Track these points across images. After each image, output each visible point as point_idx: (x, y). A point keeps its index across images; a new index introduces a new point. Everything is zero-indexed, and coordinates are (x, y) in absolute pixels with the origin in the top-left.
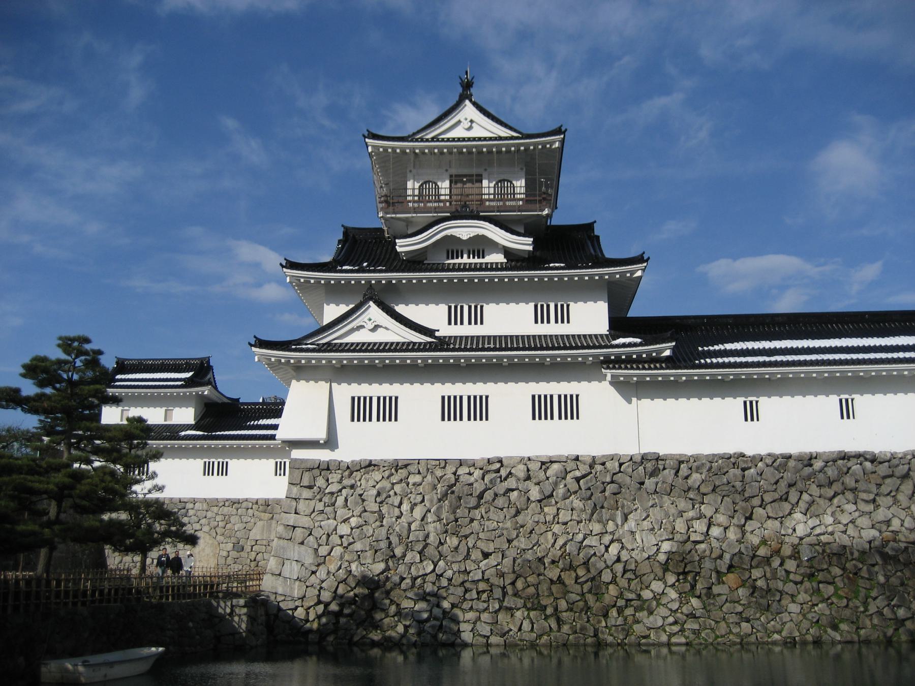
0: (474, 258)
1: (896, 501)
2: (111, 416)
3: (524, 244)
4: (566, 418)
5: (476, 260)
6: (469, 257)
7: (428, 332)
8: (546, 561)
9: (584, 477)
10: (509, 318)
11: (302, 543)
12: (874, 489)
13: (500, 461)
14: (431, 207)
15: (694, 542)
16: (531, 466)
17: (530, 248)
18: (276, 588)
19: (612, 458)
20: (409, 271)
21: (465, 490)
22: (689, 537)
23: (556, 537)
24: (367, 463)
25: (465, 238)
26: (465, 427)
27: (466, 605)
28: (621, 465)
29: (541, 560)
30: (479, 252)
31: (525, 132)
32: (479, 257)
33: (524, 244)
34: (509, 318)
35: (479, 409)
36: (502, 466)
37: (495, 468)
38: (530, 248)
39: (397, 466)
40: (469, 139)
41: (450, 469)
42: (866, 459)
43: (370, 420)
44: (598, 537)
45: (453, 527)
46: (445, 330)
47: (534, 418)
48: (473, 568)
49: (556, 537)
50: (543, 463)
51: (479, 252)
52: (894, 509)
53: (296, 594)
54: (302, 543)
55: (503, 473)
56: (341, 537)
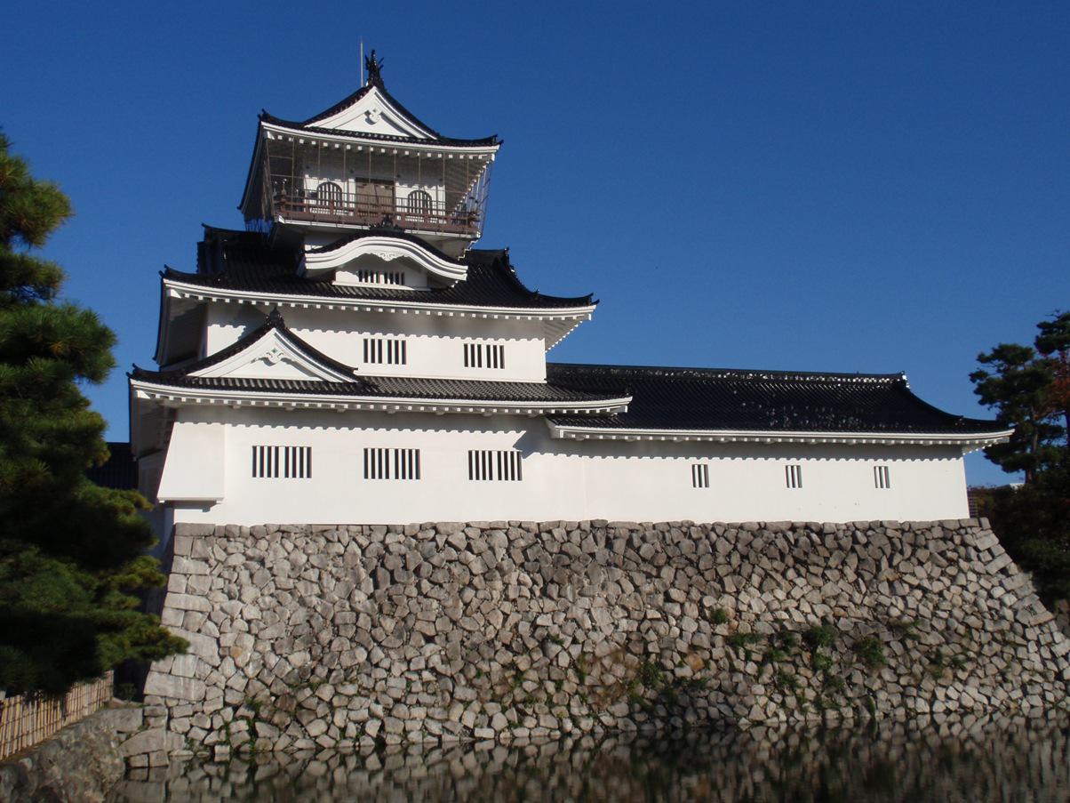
0: (392, 283)
1: (843, 575)
2: (1016, 481)
3: (459, 273)
4: (506, 478)
5: (395, 287)
6: (386, 282)
7: (347, 371)
8: (498, 644)
9: (530, 546)
10: (433, 356)
11: (199, 631)
12: (822, 563)
13: (435, 528)
14: (314, 215)
15: (651, 620)
16: (470, 532)
17: (464, 277)
18: (165, 690)
19: (558, 524)
20: (965, 432)
21: (399, 565)
22: (645, 615)
23: (506, 616)
24: (276, 529)
25: (387, 260)
26: (282, 485)
27: (412, 699)
28: (568, 533)
29: (490, 643)
30: (397, 275)
31: (443, 138)
32: (397, 283)
33: (459, 273)
34: (433, 356)
35: (409, 465)
36: (437, 532)
37: (429, 537)
38: (464, 277)
39: (310, 532)
40: (366, 136)
41: (378, 536)
42: (812, 531)
43: (387, 477)
44: (550, 616)
45: (385, 605)
46: (366, 370)
47: (366, 477)
48: (413, 655)
49: (506, 616)
50: (483, 530)
51: (397, 275)
52: (841, 584)
53: (193, 696)
54: (199, 631)
55: (441, 540)
56: (249, 622)
